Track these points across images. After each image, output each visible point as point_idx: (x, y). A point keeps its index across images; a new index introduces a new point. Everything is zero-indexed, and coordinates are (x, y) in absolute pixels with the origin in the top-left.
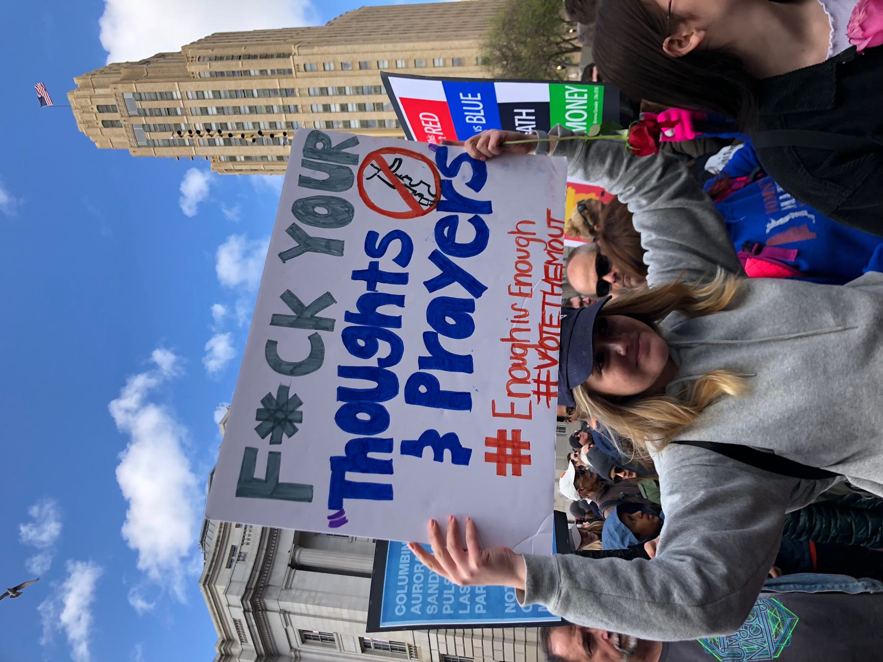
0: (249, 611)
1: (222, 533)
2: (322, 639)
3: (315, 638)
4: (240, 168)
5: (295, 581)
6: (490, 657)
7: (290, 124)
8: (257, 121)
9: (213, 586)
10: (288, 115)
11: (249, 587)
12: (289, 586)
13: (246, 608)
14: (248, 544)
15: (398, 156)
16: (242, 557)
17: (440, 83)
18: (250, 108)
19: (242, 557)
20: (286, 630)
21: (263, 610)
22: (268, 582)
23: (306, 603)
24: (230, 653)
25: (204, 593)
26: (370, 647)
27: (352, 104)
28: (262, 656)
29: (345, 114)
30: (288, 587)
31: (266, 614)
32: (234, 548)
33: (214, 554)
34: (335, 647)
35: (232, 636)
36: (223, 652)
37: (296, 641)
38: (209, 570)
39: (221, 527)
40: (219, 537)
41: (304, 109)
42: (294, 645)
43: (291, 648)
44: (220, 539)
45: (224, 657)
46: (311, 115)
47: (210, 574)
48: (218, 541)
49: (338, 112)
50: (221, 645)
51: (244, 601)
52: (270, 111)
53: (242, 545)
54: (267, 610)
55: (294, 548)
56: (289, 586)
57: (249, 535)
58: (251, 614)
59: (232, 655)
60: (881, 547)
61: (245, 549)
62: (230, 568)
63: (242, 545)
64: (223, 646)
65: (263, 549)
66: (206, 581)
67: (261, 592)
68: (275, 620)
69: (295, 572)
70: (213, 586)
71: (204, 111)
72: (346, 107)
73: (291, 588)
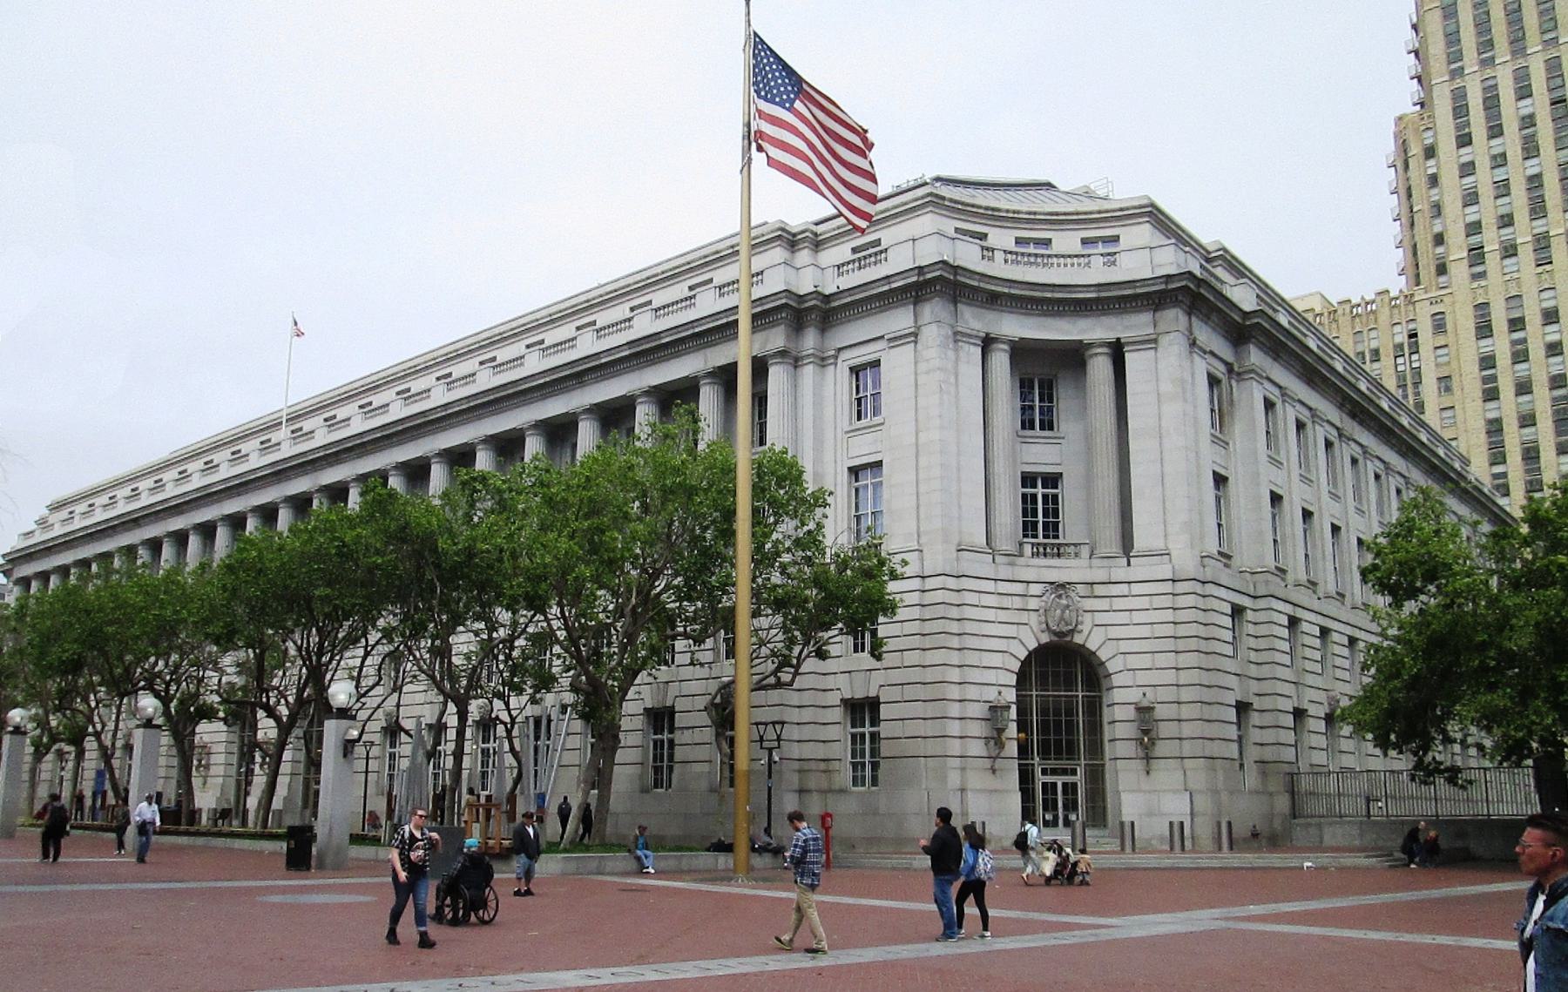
0: (919, 275)
1: (1004, 215)
2: (859, 400)
5: (966, 346)
6: (693, 675)
7: (1511, 252)
8: (1513, 192)
9: (929, 209)
10: (1530, 247)
11: (960, 271)
12: (959, 338)
13: (926, 270)
14: (1006, 261)
18: (1538, 176)
20: (882, 337)
21: (917, 296)
22: (960, 302)
24: (821, 248)
26: (857, 481)
27: (1447, 355)
28: (829, 302)
29: (1542, 352)
30: (958, 336)
31: (908, 304)
32: (1047, 243)
33: (973, 206)
34: (851, 424)
35: (799, 250)
36: (800, 237)
38: (951, 200)
39: (1014, 212)
40: (999, 210)
41: (1544, 276)
42: (845, 355)
44: (996, 213)
45: (790, 238)
46: (1535, 290)
47: (947, 203)
48: (993, 209)
49: (1543, 338)
50: (812, 232)
51: (940, 265)
52: (1536, 213)
54: (915, 304)
55: (1110, 343)
56: (959, 338)
57: (1079, 265)
58: (914, 279)
59: (817, 252)
62: (1016, 243)
63: (1102, 255)
64: (810, 235)
65: (1010, 287)
66: (937, 196)
67: (1128, 305)
68: (899, 320)
69: (1005, 350)
70: (929, 209)
71: (1524, 92)
72: (1557, 351)
73: (956, 341)
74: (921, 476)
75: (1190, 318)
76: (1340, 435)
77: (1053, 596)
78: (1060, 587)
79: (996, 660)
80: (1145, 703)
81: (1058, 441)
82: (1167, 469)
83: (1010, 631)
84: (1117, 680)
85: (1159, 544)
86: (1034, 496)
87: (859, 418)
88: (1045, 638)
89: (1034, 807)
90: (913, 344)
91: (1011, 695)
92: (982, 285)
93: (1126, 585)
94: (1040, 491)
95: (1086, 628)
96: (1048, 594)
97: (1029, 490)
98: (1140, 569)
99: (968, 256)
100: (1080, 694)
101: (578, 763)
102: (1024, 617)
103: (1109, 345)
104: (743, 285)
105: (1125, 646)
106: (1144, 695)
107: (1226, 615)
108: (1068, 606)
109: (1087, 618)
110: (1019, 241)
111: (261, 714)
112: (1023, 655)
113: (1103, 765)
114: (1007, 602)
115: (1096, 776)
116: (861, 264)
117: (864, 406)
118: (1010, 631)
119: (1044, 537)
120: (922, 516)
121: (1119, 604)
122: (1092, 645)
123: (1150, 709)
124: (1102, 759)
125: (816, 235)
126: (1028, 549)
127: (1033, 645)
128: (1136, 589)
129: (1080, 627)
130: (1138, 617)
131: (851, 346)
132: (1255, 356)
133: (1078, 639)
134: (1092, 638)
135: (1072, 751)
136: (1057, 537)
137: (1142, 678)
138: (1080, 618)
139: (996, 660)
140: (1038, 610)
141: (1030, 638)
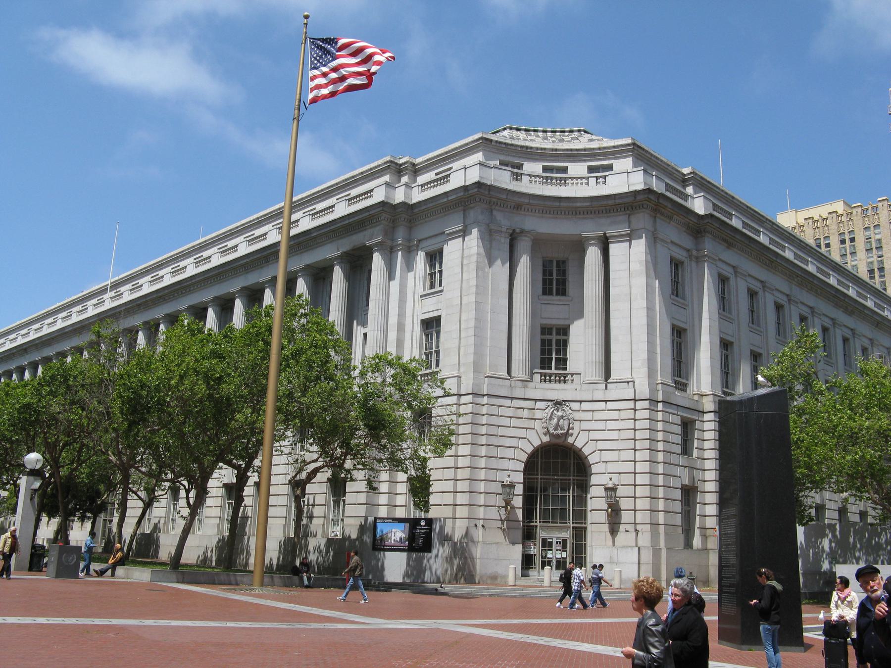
3: (676, 275)
14: (531, 181)
15: (433, 291)
16: (517, 177)
17: (680, 417)
19: (517, 177)
23: (477, 254)
25: (470, 139)
32: (564, 170)
34: (424, 290)
37: (432, 245)
43: (420, 241)
50: (411, 163)
53: (529, 175)
60: (861, 660)
61: (525, 179)
63: (529, 175)
74: (463, 326)
75: (655, 221)
76: (789, 300)
77: (553, 409)
78: (558, 404)
79: (509, 453)
80: (610, 485)
81: (567, 303)
82: (634, 323)
83: (521, 433)
84: (594, 469)
85: (627, 376)
86: (550, 341)
87: (431, 288)
88: (546, 439)
89: (573, 553)
90: (461, 239)
91: (520, 478)
92: (351, 220)
93: (604, 403)
94: (554, 338)
95: (575, 432)
96: (549, 408)
97: (548, 337)
98: (614, 392)
99: (502, 179)
100: (539, 477)
101: (405, 504)
102: (531, 424)
103: (599, 238)
104: (286, 213)
105: (600, 445)
106: (611, 479)
107: (677, 425)
108: (562, 417)
109: (577, 424)
110: (545, 169)
112: (530, 449)
113: (586, 528)
114: (519, 413)
115: (580, 534)
116: (547, 180)
117: (434, 279)
118: (521, 433)
119: (557, 368)
120: (462, 353)
121: (598, 415)
122: (579, 444)
123: (614, 489)
124: (585, 523)
125: (414, 165)
126: (537, 377)
127: (537, 443)
128: (610, 405)
129: (571, 431)
130: (611, 425)
131: (430, 237)
132: (709, 246)
133: (570, 440)
134: (579, 441)
135: (563, 514)
136: (565, 369)
137: (612, 467)
138: (571, 425)
139: (509, 453)
140: (542, 419)
141: (536, 439)
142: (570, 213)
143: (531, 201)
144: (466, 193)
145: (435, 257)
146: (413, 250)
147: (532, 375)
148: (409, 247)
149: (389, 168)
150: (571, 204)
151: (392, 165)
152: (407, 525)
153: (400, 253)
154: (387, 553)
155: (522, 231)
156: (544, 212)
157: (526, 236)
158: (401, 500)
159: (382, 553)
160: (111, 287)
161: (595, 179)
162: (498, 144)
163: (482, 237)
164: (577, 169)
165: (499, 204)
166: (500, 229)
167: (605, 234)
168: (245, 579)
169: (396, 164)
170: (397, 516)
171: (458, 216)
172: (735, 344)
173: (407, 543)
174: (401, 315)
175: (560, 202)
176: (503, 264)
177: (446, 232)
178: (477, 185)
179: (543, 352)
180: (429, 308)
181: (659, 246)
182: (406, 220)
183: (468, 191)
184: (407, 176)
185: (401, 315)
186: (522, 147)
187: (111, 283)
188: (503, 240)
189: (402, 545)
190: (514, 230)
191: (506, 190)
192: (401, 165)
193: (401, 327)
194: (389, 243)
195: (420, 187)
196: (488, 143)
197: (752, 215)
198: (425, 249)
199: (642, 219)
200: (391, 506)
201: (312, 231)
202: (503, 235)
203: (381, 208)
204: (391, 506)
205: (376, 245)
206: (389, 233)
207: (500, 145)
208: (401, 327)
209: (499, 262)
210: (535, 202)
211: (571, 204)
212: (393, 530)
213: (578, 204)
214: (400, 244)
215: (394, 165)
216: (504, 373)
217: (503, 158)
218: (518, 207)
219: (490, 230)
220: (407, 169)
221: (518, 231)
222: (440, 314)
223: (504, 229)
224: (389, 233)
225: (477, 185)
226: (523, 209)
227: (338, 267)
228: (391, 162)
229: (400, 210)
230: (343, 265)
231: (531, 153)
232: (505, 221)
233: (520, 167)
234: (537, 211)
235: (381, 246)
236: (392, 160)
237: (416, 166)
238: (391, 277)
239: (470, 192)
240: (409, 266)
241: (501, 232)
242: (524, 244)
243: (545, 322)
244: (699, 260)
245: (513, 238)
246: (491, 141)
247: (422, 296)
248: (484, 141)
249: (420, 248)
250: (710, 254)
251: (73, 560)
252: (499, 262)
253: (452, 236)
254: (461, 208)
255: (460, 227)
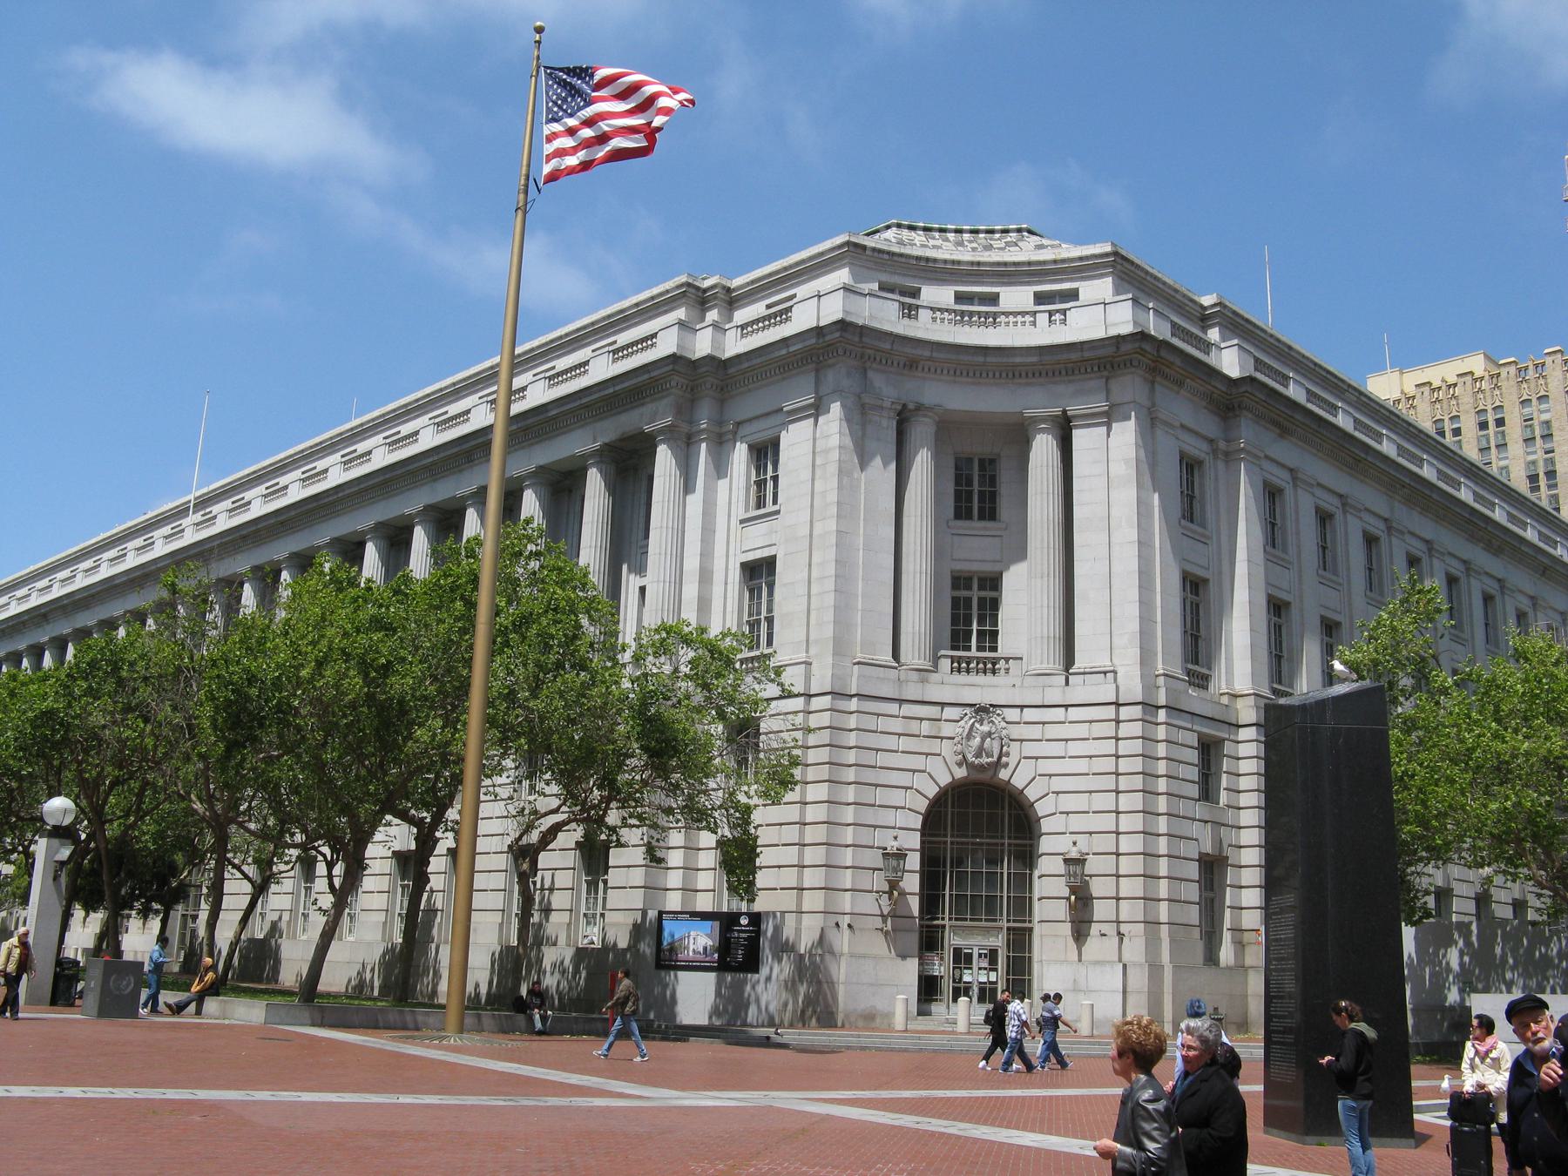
3: (1190, 484)
4: (619, 308)
14: (934, 319)
15: (762, 511)
16: (910, 311)
19: (910, 311)
23: (840, 447)
25: (828, 245)
32: (993, 299)
34: (747, 510)
37: (759, 431)
43: (738, 424)
50: (724, 287)
53: (932, 309)
56: (1311, 399)
61: (924, 315)
63: (932, 309)
65: (760, 356)
74: (814, 574)
75: (1152, 390)
76: (1389, 528)
77: (973, 720)
78: (983, 711)
79: (897, 797)
80: (1074, 854)
81: (999, 533)
82: (1116, 568)
83: (916, 762)
84: (1046, 825)
85: (1103, 662)
86: (968, 601)
87: (758, 507)
88: (961, 773)
90: (811, 420)
91: (914, 841)
93: (1063, 709)
94: (975, 594)
95: (1012, 760)
96: (967, 718)
97: (964, 593)
98: (1081, 690)
99: (884, 315)
100: (949, 840)
102: (934, 746)
103: (1053, 419)
105: (1056, 783)
106: (1075, 843)
107: (1192, 747)
108: (990, 734)
109: (1015, 746)
110: (960, 297)
111: (520, 843)
112: (932, 791)
113: (1031, 930)
114: (914, 727)
115: (1020, 940)
116: (962, 318)
117: (763, 492)
118: (916, 762)
119: (979, 649)
120: (812, 622)
121: (1052, 731)
122: (1018, 782)
123: (1080, 861)
124: (1030, 922)
125: (729, 290)
126: (945, 664)
127: (945, 780)
128: (1074, 714)
129: (1004, 759)
130: (1075, 749)
131: (757, 418)
132: (1248, 433)
133: (1004, 775)
134: (1018, 776)
135: (992, 905)
136: (994, 649)
137: (1077, 823)
138: (1005, 749)
139: (897, 797)
140: (953, 738)
141: (943, 773)
142: (1004, 375)
143: (935, 355)
144: (821, 341)
145: (765, 453)
146: (727, 441)
147: (936, 659)
148: (720, 435)
149: (685, 296)
150: (1005, 360)
151: (691, 290)
152: (717, 924)
153: (704, 446)
154: (680, 974)
155: (919, 407)
156: (958, 372)
157: (925, 416)
158: (705, 880)
159: (672, 973)
160: (195, 505)
161: (1047, 314)
162: (876, 254)
163: (848, 418)
164: (1016, 297)
165: (878, 359)
166: (880, 403)
167: (1064, 412)
168: (431, 1020)
169: (698, 288)
170: (698, 909)
171: (807, 381)
172: (1293, 605)
173: (716, 955)
174: (706, 554)
175: (985, 355)
176: (885, 464)
177: (785, 409)
178: (839, 326)
179: (955, 620)
180: (755, 542)
181: (1159, 433)
182: (714, 388)
183: (824, 336)
184: (716, 310)
185: (706, 554)
186: (918, 258)
187: (195, 499)
188: (885, 423)
189: (707, 959)
190: (904, 406)
191: (891, 334)
192: (705, 291)
193: (705, 576)
194: (685, 428)
195: (739, 329)
196: (859, 251)
197: (1324, 379)
198: (748, 439)
199: (1130, 386)
200: (689, 890)
201: (549, 407)
202: (885, 414)
203: (671, 367)
204: (689, 890)
205: (661, 431)
206: (685, 410)
207: (881, 255)
208: (705, 576)
209: (878, 461)
210: (942, 356)
211: (1005, 360)
212: (692, 933)
213: (1018, 360)
214: (704, 430)
215: (693, 291)
216: (887, 657)
217: (885, 278)
218: (912, 364)
219: (863, 406)
220: (715, 298)
221: (911, 406)
222: (774, 553)
223: (887, 404)
224: (685, 410)
225: (839, 326)
226: (920, 368)
227: (595, 470)
228: (688, 285)
229: (704, 369)
230: (604, 467)
231: (935, 270)
232: (888, 388)
233: (915, 293)
234: (945, 372)
235: (670, 434)
236: (691, 281)
237: (731, 293)
238: (688, 488)
239: (827, 338)
240: (720, 467)
241: (882, 408)
242: (922, 430)
243: (959, 566)
244: (1230, 457)
245: (904, 419)
246: (864, 248)
247: (742, 522)
248: (852, 248)
249: (738, 436)
250: (1249, 448)
251: (128, 985)
252: (878, 461)
253: (796, 415)
254: (812, 366)
255: (809, 399)
